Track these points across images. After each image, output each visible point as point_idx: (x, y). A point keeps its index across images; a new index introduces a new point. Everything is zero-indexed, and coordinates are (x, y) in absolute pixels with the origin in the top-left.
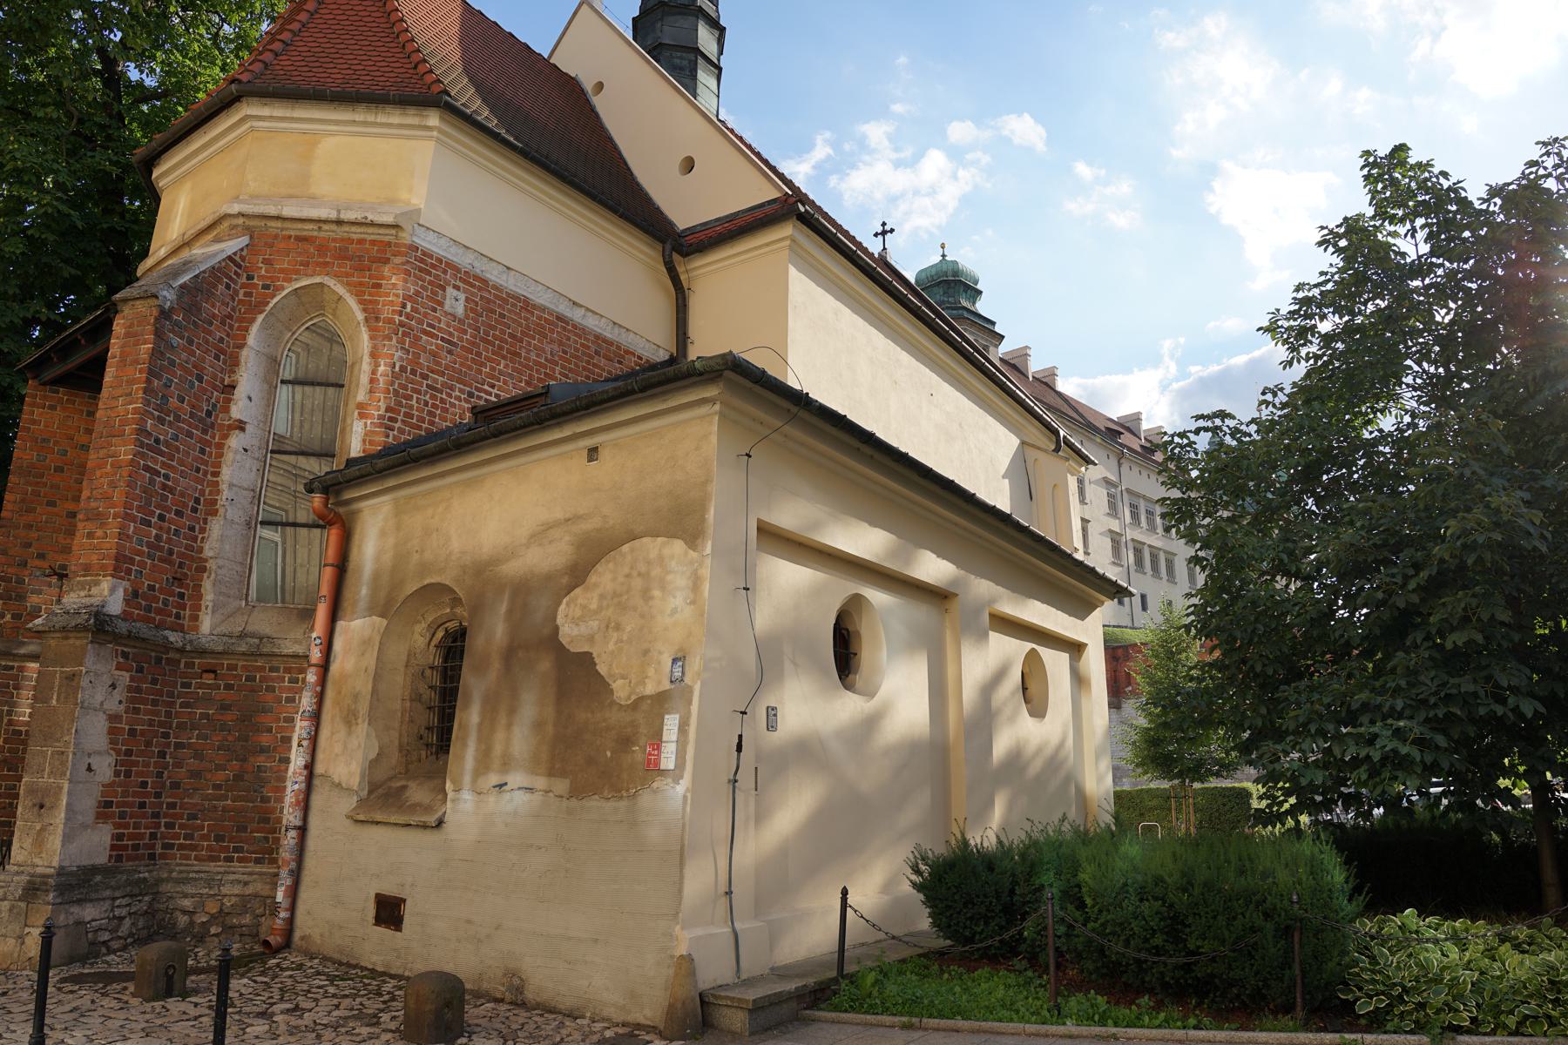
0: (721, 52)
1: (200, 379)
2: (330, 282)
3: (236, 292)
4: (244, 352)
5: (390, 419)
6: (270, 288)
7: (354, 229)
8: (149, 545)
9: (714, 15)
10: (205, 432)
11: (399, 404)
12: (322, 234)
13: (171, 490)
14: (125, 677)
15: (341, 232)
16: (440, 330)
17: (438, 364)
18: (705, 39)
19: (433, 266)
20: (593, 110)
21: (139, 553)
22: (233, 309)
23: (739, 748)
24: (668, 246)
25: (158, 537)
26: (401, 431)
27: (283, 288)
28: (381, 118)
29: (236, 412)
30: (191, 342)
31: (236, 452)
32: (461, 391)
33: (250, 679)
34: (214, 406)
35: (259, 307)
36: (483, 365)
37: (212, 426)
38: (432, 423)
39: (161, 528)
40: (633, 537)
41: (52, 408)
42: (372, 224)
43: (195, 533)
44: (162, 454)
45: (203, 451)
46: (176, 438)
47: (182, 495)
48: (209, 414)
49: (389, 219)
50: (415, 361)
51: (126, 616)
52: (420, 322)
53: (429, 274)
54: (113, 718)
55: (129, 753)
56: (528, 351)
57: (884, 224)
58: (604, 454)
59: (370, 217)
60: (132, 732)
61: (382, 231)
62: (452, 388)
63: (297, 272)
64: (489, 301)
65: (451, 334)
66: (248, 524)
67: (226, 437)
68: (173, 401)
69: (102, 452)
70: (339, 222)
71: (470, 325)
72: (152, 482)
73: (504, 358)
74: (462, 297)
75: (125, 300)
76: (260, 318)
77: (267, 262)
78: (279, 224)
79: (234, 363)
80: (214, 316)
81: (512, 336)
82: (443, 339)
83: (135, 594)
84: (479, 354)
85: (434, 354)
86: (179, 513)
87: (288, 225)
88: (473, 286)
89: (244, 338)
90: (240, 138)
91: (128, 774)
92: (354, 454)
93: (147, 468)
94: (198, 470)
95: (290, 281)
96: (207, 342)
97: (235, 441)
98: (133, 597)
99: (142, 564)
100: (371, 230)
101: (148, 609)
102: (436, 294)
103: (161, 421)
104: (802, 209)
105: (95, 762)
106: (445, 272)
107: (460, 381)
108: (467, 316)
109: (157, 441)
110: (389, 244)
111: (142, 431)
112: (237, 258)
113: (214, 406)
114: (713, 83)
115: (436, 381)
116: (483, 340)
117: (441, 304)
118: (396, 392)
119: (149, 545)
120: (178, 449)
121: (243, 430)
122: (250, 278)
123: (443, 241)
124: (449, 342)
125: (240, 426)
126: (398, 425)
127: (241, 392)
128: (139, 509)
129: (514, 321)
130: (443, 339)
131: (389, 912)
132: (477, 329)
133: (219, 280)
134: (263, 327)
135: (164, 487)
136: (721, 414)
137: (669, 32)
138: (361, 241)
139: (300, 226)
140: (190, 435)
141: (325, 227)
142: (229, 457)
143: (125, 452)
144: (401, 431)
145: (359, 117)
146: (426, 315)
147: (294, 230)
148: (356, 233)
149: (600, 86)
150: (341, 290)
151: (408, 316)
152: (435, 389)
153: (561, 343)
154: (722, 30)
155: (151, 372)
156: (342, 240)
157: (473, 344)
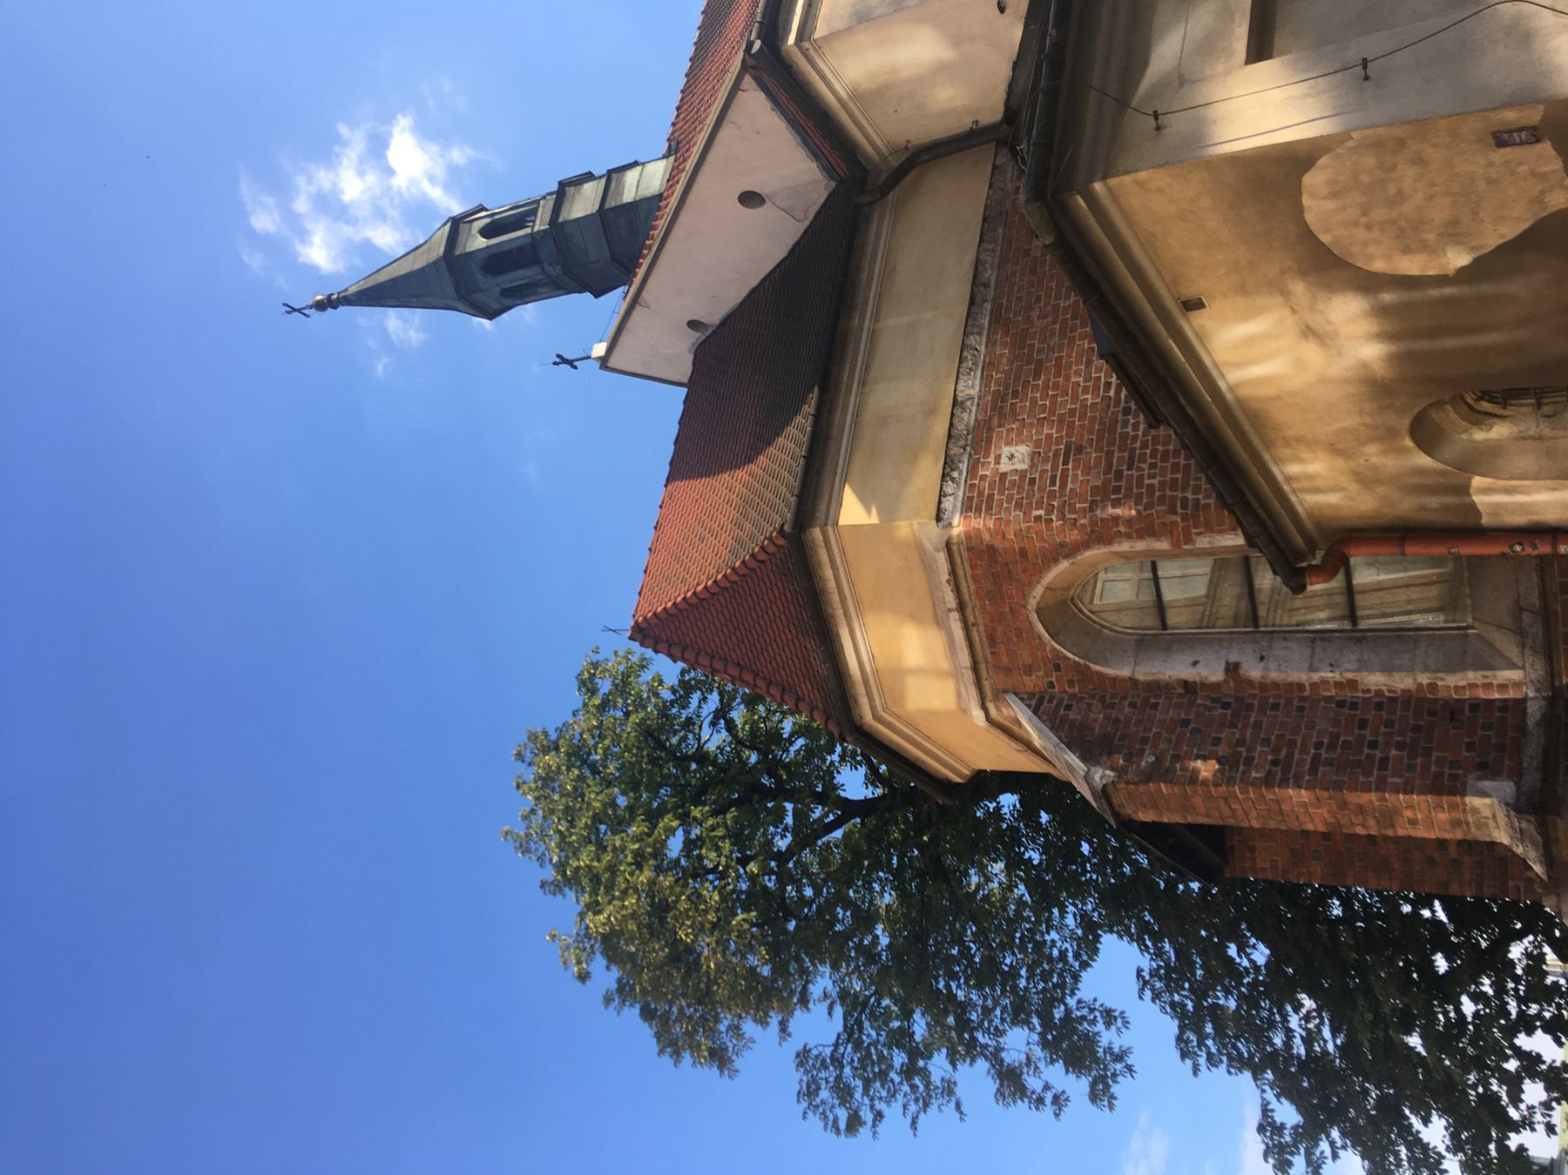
0: (589, 177)
1: (1186, 723)
2: (1032, 603)
3: (1072, 697)
4: (1141, 677)
5: (1184, 506)
6: (1057, 664)
7: (965, 590)
8: (1412, 756)
9: (551, 201)
10: (1250, 707)
11: (1162, 499)
12: (980, 621)
16: (1054, 468)
18: (584, 204)
19: (981, 493)
20: (724, 323)
21: (1426, 767)
22: (1093, 697)
24: (866, 199)
25: (1400, 746)
26: (1197, 490)
28: (832, 584)
30: (1145, 740)
31: (1266, 669)
32: (1125, 424)
34: (1214, 700)
35: (1083, 674)
36: (1084, 405)
37: (1239, 699)
38: (1177, 453)
39: (1388, 745)
40: (1307, 234)
41: (1252, 850)
42: (953, 572)
44: (1290, 756)
45: (1275, 706)
46: (1266, 741)
48: (1226, 706)
49: (942, 558)
51: (1516, 775)
53: (991, 496)
58: (1190, 292)
59: (945, 577)
61: (958, 560)
62: (1124, 437)
65: (1056, 454)
66: (1359, 640)
67: (1250, 682)
69: (1302, 818)
70: (961, 607)
73: (1067, 379)
74: (1006, 451)
75: (1116, 814)
78: (982, 667)
79: (1156, 687)
80: (1107, 718)
82: (1066, 463)
84: (1072, 412)
86: (1363, 724)
87: (980, 657)
89: (1124, 680)
90: (898, 717)
92: (1240, 541)
93: (1313, 770)
94: (1301, 709)
95: (1043, 644)
96: (1139, 721)
97: (1254, 671)
100: (961, 573)
102: (1013, 483)
103: (1249, 761)
104: (757, 45)
106: (983, 478)
109: (1275, 763)
111: (1268, 781)
112: (1033, 703)
113: (1214, 700)
114: (631, 176)
115: (1121, 459)
117: (1023, 474)
119: (1412, 756)
120: (1281, 737)
121: (1236, 666)
125: (1232, 669)
126: (1190, 496)
128: (1368, 773)
130: (1066, 463)
132: (1041, 421)
133: (1064, 719)
134: (1106, 663)
135: (1332, 747)
136: (1104, 178)
137: (596, 251)
139: (978, 646)
141: (971, 619)
142: (1275, 675)
143: (1297, 796)
144: (1197, 490)
145: (836, 597)
147: (983, 651)
148: (967, 586)
149: (693, 324)
150: (1038, 591)
151: (1050, 511)
152: (1131, 458)
154: (563, 185)
156: (980, 599)
157: (1061, 421)
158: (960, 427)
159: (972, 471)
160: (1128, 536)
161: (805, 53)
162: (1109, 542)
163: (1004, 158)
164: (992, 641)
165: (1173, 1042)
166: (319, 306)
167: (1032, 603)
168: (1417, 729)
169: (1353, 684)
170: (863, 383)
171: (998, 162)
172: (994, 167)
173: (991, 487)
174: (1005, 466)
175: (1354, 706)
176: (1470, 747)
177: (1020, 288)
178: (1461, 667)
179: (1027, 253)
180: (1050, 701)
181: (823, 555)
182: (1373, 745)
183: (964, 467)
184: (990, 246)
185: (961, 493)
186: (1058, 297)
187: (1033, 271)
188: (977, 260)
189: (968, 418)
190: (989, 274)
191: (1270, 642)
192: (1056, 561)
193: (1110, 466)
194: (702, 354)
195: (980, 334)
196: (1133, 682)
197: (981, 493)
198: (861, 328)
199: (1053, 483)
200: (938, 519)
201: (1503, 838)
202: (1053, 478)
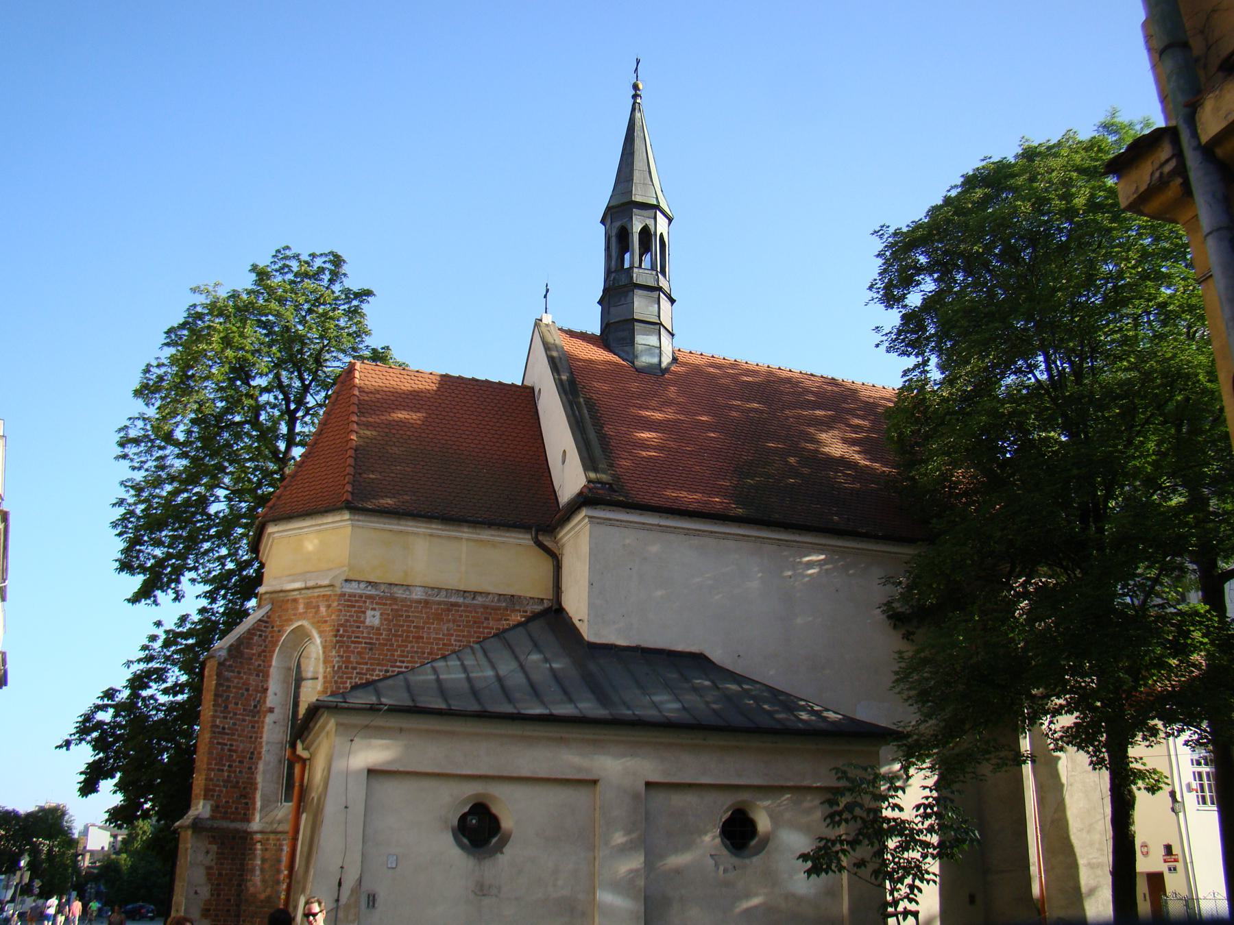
1: (247, 690)
13: (235, 751)
14: (214, 848)
23: (340, 884)
29: (269, 704)
42: (320, 587)
43: (251, 771)
45: (253, 727)
46: (235, 724)
47: (243, 752)
49: (326, 582)
50: (348, 661)
51: (212, 818)
52: (349, 637)
54: (209, 868)
55: (219, 885)
60: (220, 874)
62: (374, 670)
64: (397, 610)
66: (280, 761)
68: (231, 706)
72: (223, 749)
74: (377, 614)
77: (280, 617)
79: (266, 676)
83: (218, 807)
84: (392, 645)
88: (385, 604)
91: (219, 895)
97: (269, 719)
98: (215, 809)
99: (221, 791)
101: (226, 812)
103: (225, 718)
105: (199, 889)
107: (378, 664)
116: (396, 636)
117: (364, 622)
118: (336, 682)
123: (362, 585)
125: (271, 710)
127: (270, 692)
131: (479, 829)
140: (244, 720)
145: (320, 522)
151: (341, 636)
153: (454, 621)
155: (216, 695)
158: (395, 589)
163: (546, 604)
165: (971, 164)
166: (636, 87)
168: (237, 782)
169: (260, 758)
170: (431, 535)
174: (369, 613)
175: (251, 758)
176: (227, 802)
178: (262, 800)
179: (487, 619)
181: (338, 518)
182: (230, 766)
183: (373, 592)
189: (399, 593)
190: (480, 600)
196: (270, 666)
200: (346, 581)
201: (190, 813)
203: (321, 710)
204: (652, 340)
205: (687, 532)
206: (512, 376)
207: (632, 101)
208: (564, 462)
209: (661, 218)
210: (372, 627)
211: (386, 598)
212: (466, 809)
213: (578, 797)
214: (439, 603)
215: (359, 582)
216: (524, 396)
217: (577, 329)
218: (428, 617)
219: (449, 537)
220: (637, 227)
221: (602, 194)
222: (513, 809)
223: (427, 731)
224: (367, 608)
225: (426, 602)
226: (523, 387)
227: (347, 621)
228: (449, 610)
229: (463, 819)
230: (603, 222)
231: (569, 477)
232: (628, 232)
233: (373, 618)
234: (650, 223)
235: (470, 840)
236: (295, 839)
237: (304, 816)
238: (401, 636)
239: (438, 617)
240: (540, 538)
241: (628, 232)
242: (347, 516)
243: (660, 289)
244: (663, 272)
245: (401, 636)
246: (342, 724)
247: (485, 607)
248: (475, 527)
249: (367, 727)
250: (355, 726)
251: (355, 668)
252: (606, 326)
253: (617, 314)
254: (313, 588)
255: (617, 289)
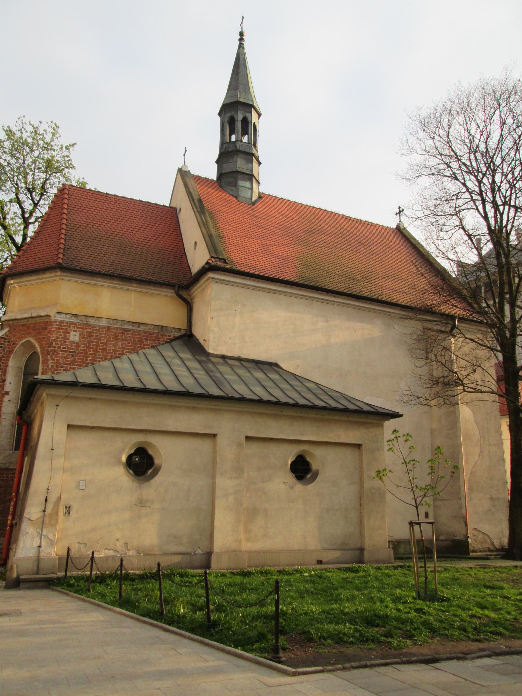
12: (29, 323)
15: (33, 321)
16: (68, 348)
17: (68, 361)
19: (64, 326)
27: (18, 344)
28: (44, 276)
33: (7, 477)
42: (41, 316)
53: (62, 329)
56: (110, 347)
57: (399, 208)
63: (22, 337)
64: (90, 332)
65: (73, 349)
66: (12, 425)
70: (32, 318)
71: (82, 344)
73: (98, 352)
74: (78, 334)
76: (12, 355)
81: (101, 343)
82: (69, 352)
85: (65, 358)
88: (83, 328)
95: (20, 341)
97: (6, 398)
100: (41, 318)
106: (70, 327)
107: (77, 365)
108: (80, 340)
110: (47, 322)
115: (67, 367)
116: (88, 347)
117: (68, 339)
121: (8, 394)
122: (9, 342)
123: (68, 316)
124: (72, 352)
125: (7, 393)
129: (102, 337)
130: (69, 352)
131: (301, 469)
138: (39, 323)
141: (30, 320)
145: (41, 277)
146: (61, 345)
148: (38, 320)
151: (54, 347)
153: (126, 340)
157: (84, 350)
159: (72, 323)
160: (43, 369)
161: (208, 280)
162: (43, 363)
163: (183, 332)
164: (23, 325)
166: (241, 34)
167: (33, 341)
170: (112, 287)
171: (182, 330)
172: (180, 329)
173: (66, 329)
174: (72, 333)
177: (134, 338)
179: (146, 339)
180: (4, 342)
181: (53, 274)
184: (152, 328)
185: (66, 320)
186: (128, 349)
187: (139, 341)
188: (148, 324)
189: (92, 322)
190: (142, 328)
191: (15, 403)
192: (40, 347)
193: (65, 364)
194: (175, 209)
195: (121, 325)
197: (64, 326)
198: (133, 287)
199: (63, 348)
202: (65, 348)
203: (39, 385)
204: (247, 184)
205: (269, 291)
206: (164, 200)
207: (238, 43)
208: (195, 248)
209: (254, 114)
210: (74, 342)
211: (84, 325)
212: (132, 451)
213: (205, 445)
214: (117, 329)
215: (66, 314)
216: (171, 214)
217: (246, 43)
218: (110, 338)
219: (124, 289)
220: (240, 117)
221: (219, 96)
222: (164, 450)
223: (109, 401)
224: (71, 330)
225: (109, 328)
226: (170, 207)
227: (57, 338)
228: (123, 333)
229: (130, 458)
230: (220, 114)
231: (198, 257)
232: (237, 114)
233: (74, 337)
234: (248, 115)
235: (134, 472)
236: (21, 473)
237: (26, 458)
238: (93, 348)
239: (116, 338)
240: (180, 292)
241: (237, 114)
242: (59, 273)
243: (253, 155)
244: (255, 145)
245: (93, 348)
246: (50, 395)
247: (145, 332)
248: (140, 284)
249: (67, 397)
250: (59, 396)
251: (62, 367)
252: (221, 175)
253: (228, 168)
254: (37, 317)
255: (228, 154)
